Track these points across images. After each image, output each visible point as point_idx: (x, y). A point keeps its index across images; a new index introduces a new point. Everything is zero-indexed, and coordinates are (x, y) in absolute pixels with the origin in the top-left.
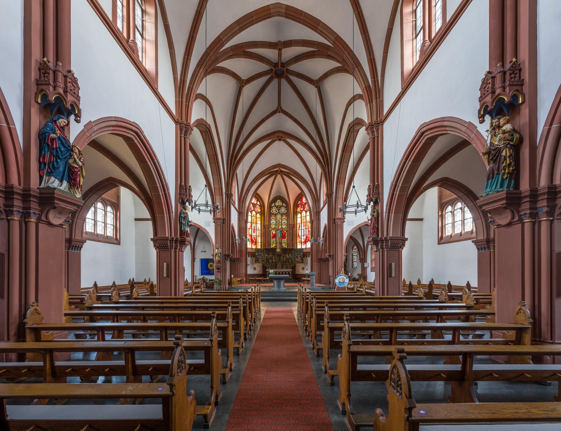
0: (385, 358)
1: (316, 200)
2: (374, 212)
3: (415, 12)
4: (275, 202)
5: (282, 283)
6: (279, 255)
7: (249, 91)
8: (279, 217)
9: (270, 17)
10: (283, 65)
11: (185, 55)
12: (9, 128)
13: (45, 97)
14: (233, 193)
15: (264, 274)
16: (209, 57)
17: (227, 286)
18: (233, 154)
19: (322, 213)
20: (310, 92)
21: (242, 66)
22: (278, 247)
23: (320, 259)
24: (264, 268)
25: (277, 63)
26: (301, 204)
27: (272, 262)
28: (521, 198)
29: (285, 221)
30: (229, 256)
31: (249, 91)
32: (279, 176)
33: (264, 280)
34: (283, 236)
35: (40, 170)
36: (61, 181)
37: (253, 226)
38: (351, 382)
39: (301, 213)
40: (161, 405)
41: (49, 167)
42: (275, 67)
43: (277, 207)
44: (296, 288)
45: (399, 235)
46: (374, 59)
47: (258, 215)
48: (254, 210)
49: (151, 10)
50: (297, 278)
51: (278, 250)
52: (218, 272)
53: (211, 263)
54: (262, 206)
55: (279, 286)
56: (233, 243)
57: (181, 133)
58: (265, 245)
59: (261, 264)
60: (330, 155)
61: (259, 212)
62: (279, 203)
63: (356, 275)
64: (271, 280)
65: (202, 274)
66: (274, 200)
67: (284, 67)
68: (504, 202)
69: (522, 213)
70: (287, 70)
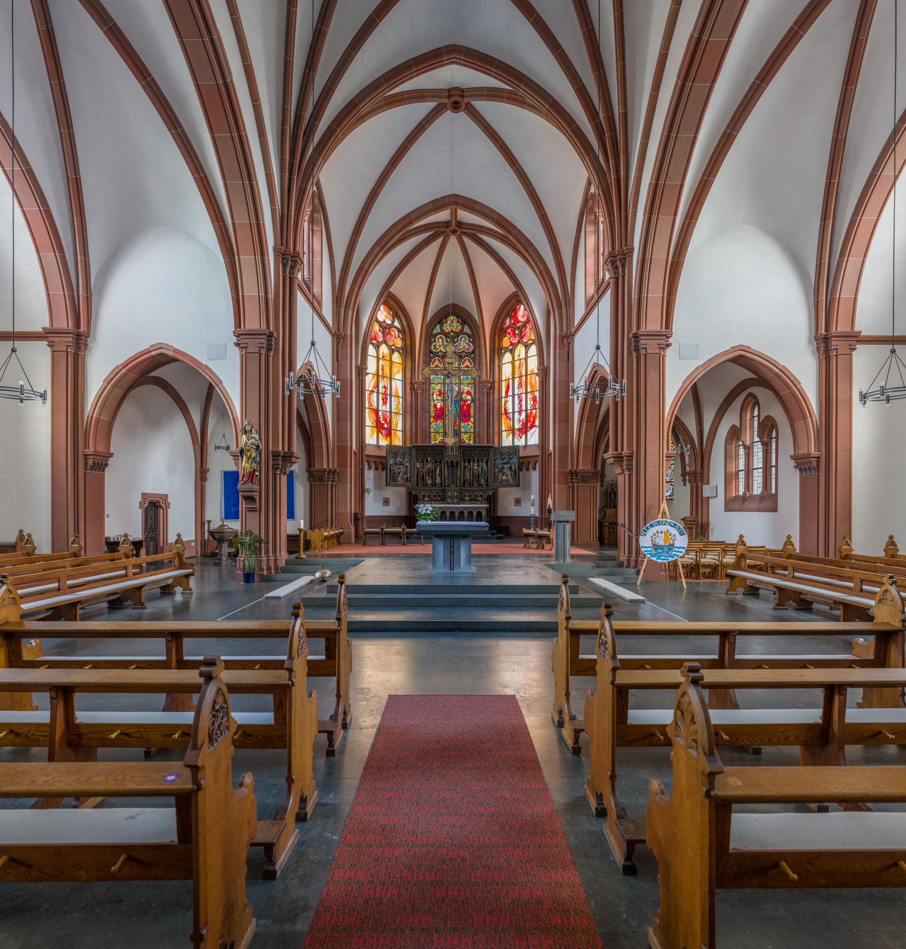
1: (561, 301)
4: (440, 322)
6: (453, 465)
15: (410, 519)
24: (413, 500)
27: (434, 484)
32: (453, 240)
34: (464, 415)
37: (381, 385)
38: (570, 677)
39: (512, 352)
40: (174, 809)
43: (447, 335)
47: (396, 357)
48: (385, 342)
52: (252, 510)
54: (407, 332)
59: (403, 490)
62: (452, 324)
66: (441, 317)
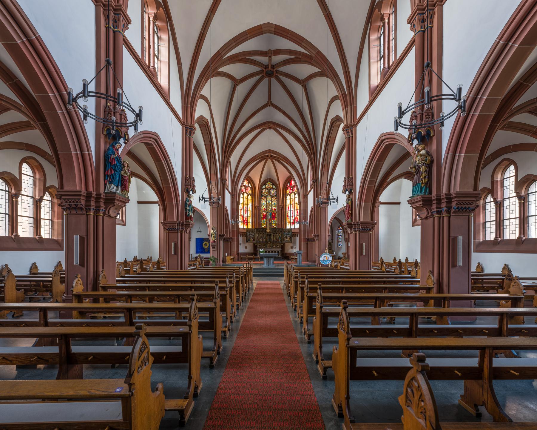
0: (314, 290)
1: (304, 184)
2: (349, 200)
3: (379, 38)
4: (265, 185)
5: (271, 260)
6: (269, 235)
7: (242, 89)
8: (269, 198)
9: (262, 34)
10: (273, 67)
11: (190, 68)
12: (89, 154)
13: (108, 130)
14: (227, 178)
15: (255, 253)
16: (210, 69)
17: (222, 264)
18: (227, 143)
19: (309, 196)
20: (298, 90)
21: (236, 70)
22: (268, 228)
23: (308, 239)
24: (255, 247)
25: (268, 65)
26: (290, 186)
28: (431, 201)
29: (275, 203)
30: (223, 236)
31: (242, 89)
32: (269, 161)
33: (255, 259)
35: (105, 180)
36: (117, 187)
39: (290, 195)
41: (110, 177)
42: (265, 68)
43: (267, 189)
44: (283, 265)
45: (368, 220)
46: (349, 72)
47: (250, 197)
48: (246, 192)
49: (164, 36)
50: (285, 256)
51: (268, 231)
53: (206, 242)
54: (253, 188)
55: (268, 263)
56: (226, 224)
57: (186, 133)
58: (255, 225)
59: (252, 244)
60: (316, 144)
61: (250, 194)
62: (269, 185)
63: (340, 254)
64: (262, 258)
65: (197, 252)
66: (265, 183)
67: (274, 68)
68: (421, 203)
69: (433, 211)
70: (277, 71)
